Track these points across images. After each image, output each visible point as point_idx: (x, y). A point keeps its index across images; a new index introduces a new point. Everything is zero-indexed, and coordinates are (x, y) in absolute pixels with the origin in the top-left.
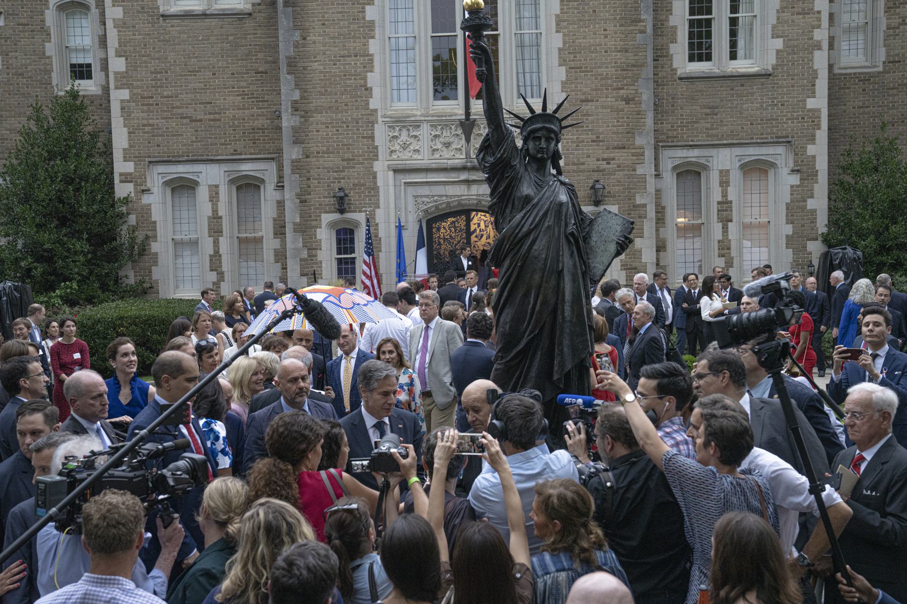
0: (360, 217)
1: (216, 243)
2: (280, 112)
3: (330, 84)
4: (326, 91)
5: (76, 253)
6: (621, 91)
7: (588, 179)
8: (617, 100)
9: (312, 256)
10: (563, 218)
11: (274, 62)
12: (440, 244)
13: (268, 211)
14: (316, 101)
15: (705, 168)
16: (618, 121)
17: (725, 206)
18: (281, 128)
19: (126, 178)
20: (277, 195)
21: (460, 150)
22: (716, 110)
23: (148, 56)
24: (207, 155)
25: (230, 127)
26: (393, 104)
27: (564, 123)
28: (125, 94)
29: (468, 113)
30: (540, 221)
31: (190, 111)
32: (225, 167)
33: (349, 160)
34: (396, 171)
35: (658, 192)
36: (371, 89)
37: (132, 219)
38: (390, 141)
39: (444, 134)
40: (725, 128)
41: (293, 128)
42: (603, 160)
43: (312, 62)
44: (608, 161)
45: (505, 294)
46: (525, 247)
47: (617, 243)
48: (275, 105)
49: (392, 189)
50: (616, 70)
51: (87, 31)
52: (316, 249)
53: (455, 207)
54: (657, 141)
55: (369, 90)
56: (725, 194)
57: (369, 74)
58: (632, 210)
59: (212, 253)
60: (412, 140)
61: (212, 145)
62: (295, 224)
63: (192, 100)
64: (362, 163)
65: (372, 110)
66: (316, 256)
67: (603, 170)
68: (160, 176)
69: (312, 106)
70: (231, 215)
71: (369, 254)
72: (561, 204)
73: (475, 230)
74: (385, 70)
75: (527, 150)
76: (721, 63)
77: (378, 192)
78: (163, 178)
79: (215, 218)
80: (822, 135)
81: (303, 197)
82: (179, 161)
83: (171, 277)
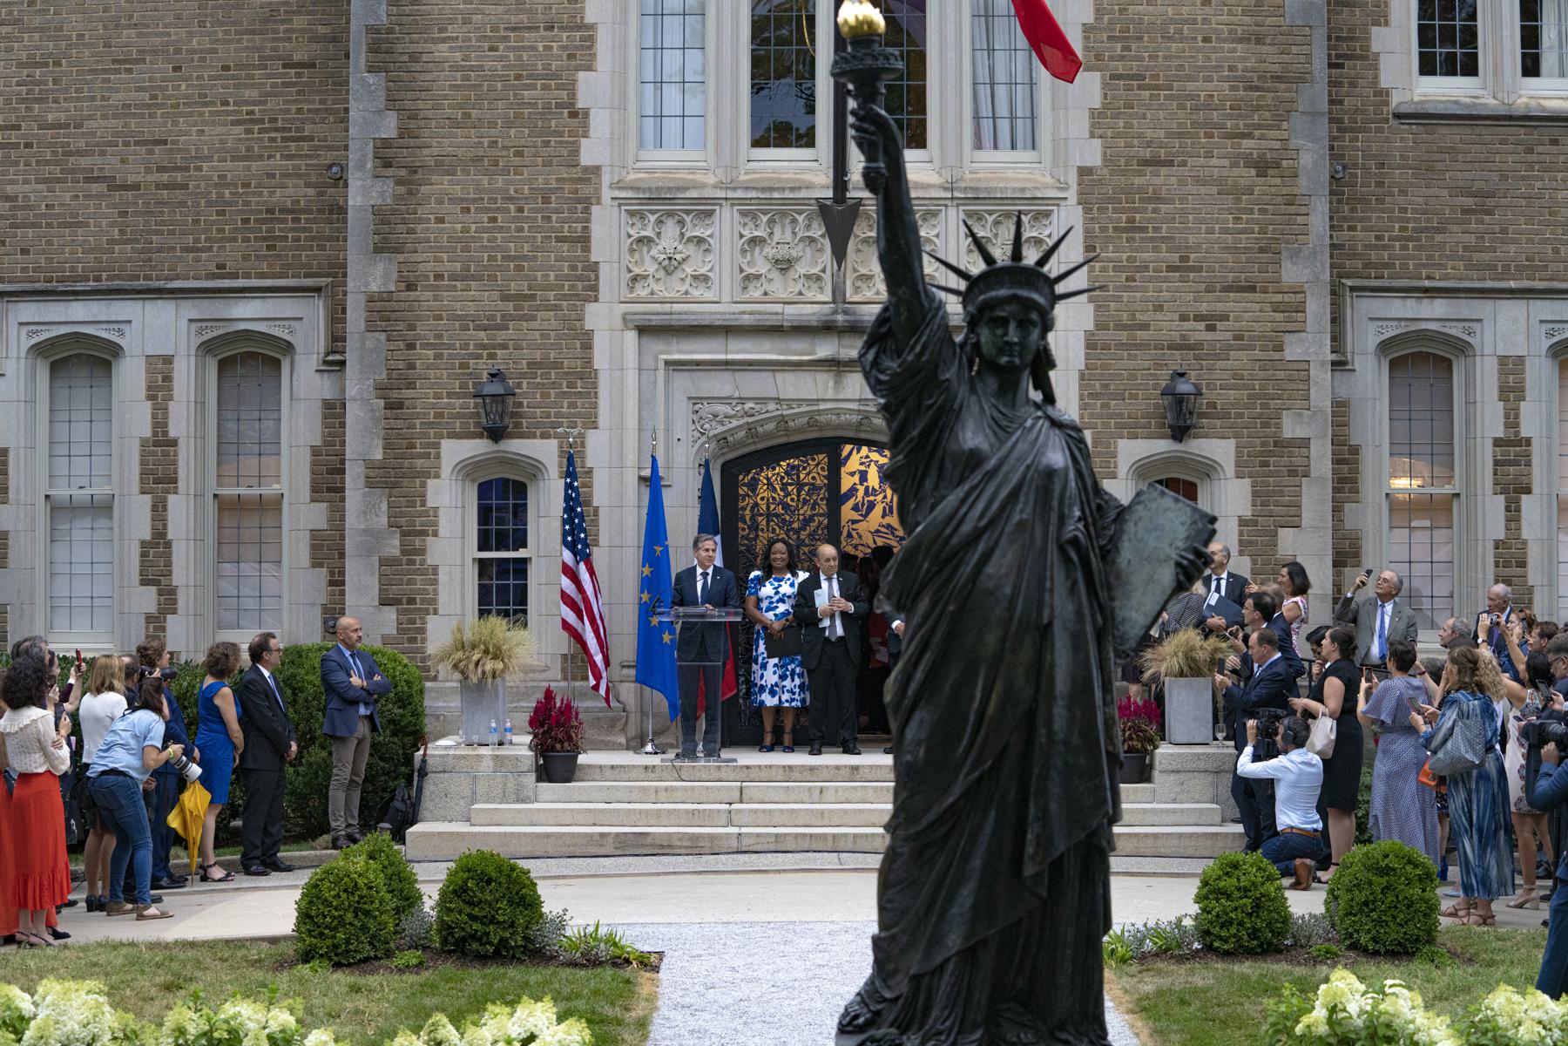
0: (545, 451)
1: (159, 510)
2: (343, 169)
3: (478, 98)
4: (467, 116)
6: (1247, 143)
7: (1158, 366)
8: (1234, 165)
9: (413, 552)
10: (1055, 503)
11: (334, 40)
12: (755, 527)
13: (298, 427)
14: (441, 143)
15: (1463, 348)
16: (1237, 219)
17: (1513, 453)
18: (342, 210)
20: (324, 387)
21: (818, 278)
22: (1490, 202)
23: (17, 22)
24: (147, 278)
25: (209, 204)
26: (643, 155)
27: (1060, 288)
30: (1002, 508)
31: (109, 164)
32: (191, 309)
33: (520, 297)
34: (644, 330)
35: (1341, 409)
36: (586, 113)
38: (632, 251)
39: (777, 237)
40: (1513, 248)
41: (377, 211)
42: (1198, 318)
43: (434, 41)
44: (1211, 321)
45: (919, 675)
46: (967, 569)
47: (1178, 565)
48: (330, 148)
49: (631, 378)
50: (1232, 88)
52: (424, 533)
53: (798, 430)
54: (1339, 273)
55: (579, 116)
56: (1512, 421)
57: (581, 75)
58: (1270, 454)
59: (148, 536)
60: (690, 250)
61: (160, 250)
62: (370, 465)
63: (117, 134)
64: (556, 308)
65: (586, 169)
66: (422, 552)
67: (1198, 346)
68: (24, 330)
69: (427, 156)
70: (201, 438)
71: (572, 547)
72: (1050, 473)
73: (853, 490)
74: (625, 65)
75: (977, 346)
76: (1496, 84)
77: (595, 385)
78: (30, 334)
79: (161, 443)
81: (395, 394)
82: (76, 293)
83: (40, 597)
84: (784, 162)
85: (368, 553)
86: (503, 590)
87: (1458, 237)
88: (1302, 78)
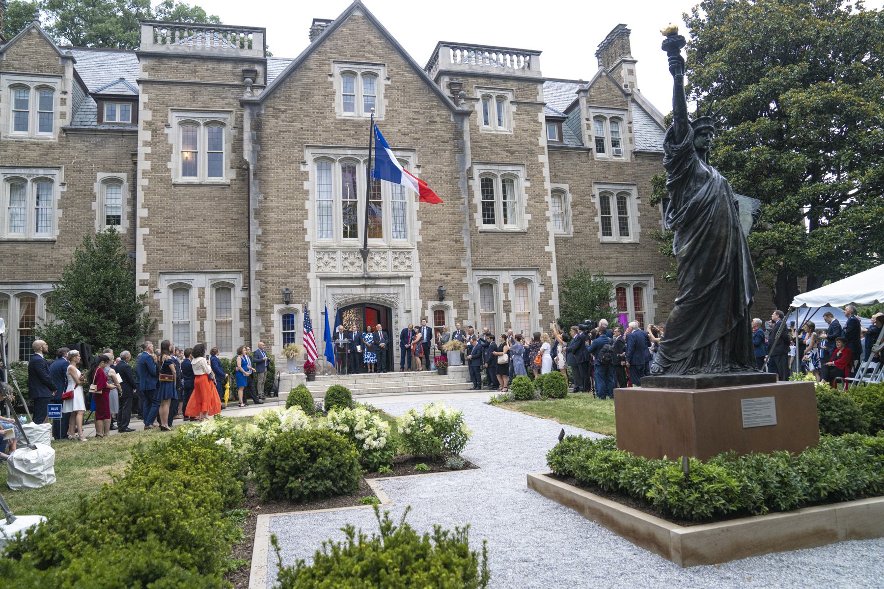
0: (299, 307)
1: (202, 324)
5: (110, 330)
9: (268, 331)
14: (272, 236)
17: (507, 303)
19: (144, 283)
28: (146, 231)
29: (365, 245)
31: (188, 242)
32: (209, 276)
34: (321, 279)
37: (147, 309)
41: (257, 251)
44: (447, 275)
51: (119, 196)
55: (305, 230)
56: (507, 297)
62: (257, 311)
69: (269, 239)
70: (212, 307)
79: (202, 309)
80: (554, 265)
84: (350, 241)
85: (257, 331)
86: (288, 338)
87: (494, 258)
88: (464, 222)
